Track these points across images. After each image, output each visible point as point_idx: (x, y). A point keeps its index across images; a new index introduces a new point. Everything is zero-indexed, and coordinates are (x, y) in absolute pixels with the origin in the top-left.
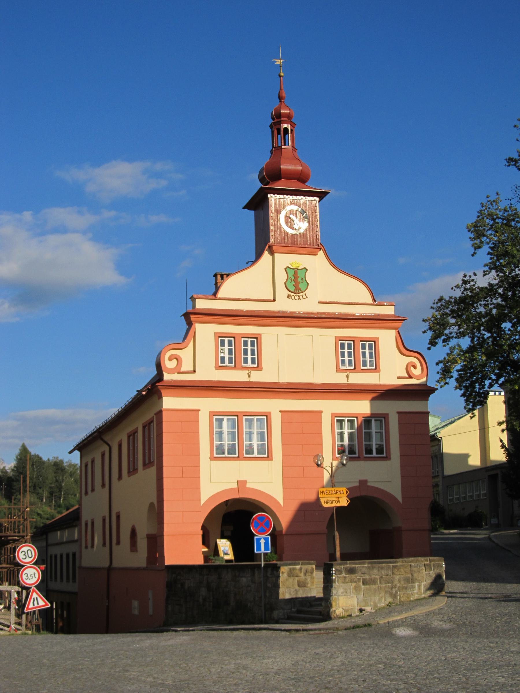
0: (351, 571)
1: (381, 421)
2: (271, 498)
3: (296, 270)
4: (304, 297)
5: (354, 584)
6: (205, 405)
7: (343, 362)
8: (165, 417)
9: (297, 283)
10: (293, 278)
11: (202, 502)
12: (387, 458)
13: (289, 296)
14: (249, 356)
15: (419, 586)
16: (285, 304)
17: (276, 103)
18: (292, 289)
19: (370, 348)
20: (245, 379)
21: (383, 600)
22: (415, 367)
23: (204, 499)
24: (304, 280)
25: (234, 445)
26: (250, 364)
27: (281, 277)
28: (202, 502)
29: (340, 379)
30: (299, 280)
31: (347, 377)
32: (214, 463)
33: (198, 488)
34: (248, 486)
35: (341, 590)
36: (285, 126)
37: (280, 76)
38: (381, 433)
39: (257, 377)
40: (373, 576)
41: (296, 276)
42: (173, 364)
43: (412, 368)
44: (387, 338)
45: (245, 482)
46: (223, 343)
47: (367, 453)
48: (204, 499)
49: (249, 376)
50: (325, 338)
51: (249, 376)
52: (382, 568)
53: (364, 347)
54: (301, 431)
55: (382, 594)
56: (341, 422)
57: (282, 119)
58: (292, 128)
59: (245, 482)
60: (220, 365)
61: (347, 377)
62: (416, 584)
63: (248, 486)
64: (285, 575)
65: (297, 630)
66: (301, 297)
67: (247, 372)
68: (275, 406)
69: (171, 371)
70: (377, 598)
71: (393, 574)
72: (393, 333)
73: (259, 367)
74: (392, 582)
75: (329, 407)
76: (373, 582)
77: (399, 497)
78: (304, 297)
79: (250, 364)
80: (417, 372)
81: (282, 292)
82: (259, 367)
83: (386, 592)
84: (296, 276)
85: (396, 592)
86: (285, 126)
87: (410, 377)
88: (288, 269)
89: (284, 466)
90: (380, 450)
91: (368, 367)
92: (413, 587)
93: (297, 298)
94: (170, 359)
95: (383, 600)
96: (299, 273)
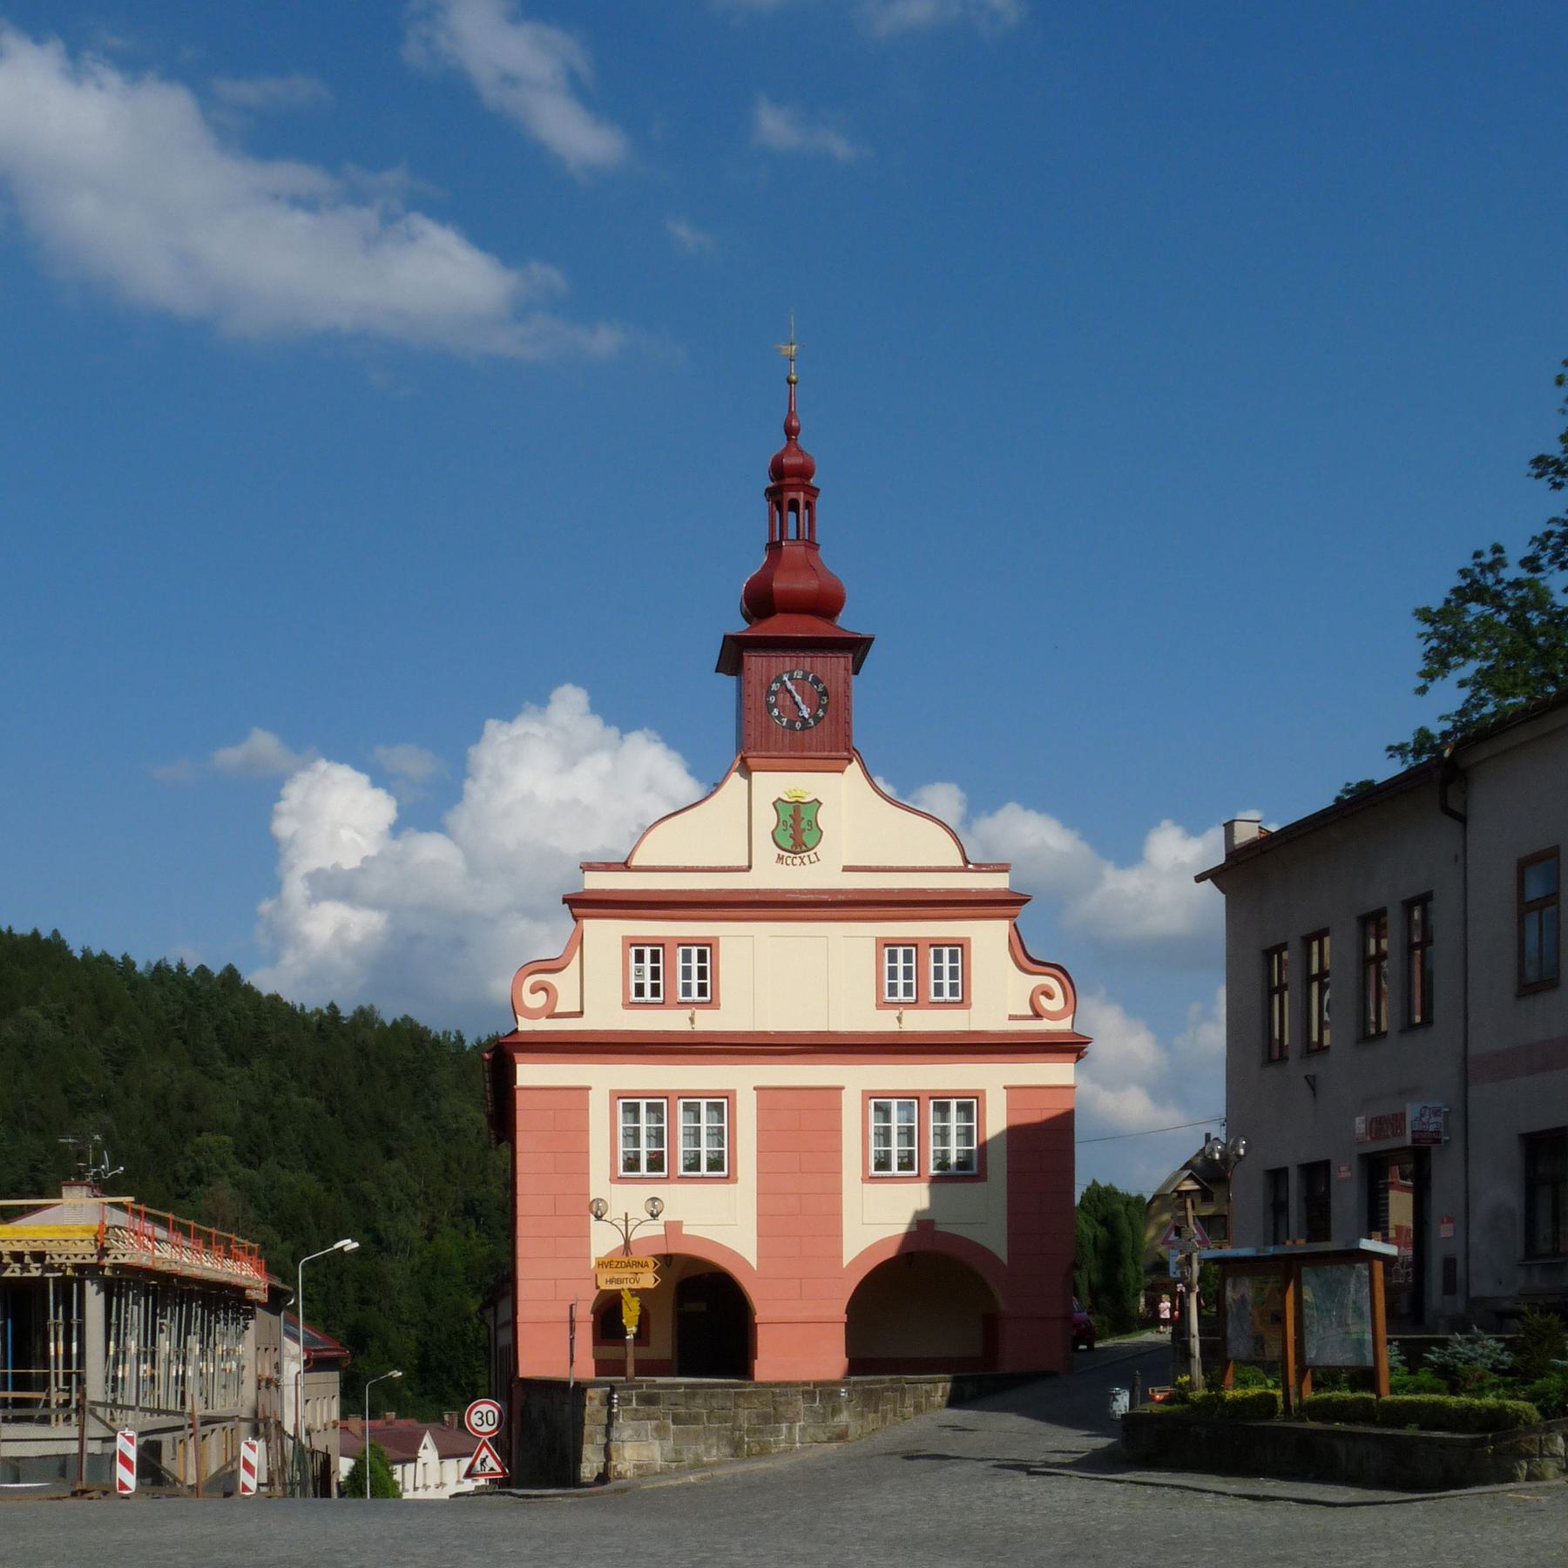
0: (649, 1400)
1: (911, 1104)
2: (733, 1254)
3: (797, 806)
4: (813, 858)
5: (654, 1423)
6: (602, 1080)
7: (893, 990)
8: (521, 1101)
9: (798, 829)
10: (790, 822)
11: (846, 1260)
12: (730, 1179)
13: (780, 858)
14: (901, 981)
15: (790, 1429)
16: (773, 874)
17: (782, 441)
18: (788, 843)
19: (953, 958)
20: (685, 1026)
21: (714, 1452)
22: (1049, 995)
23: (847, 1258)
24: (813, 824)
25: (911, 1153)
26: (901, 996)
27: (766, 820)
28: (846, 1260)
29: (885, 1023)
30: (804, 825)
31: (899, 1019)
32: (869, 1187)
33: (838, 1235)
34: (685, 1231)
35: (627, 1433)
36: (792, 495)
37: (790, 382)
38: (911, 1129)
39: (707, 1022)
40: (695, 1410)
41: (796, 817)
42: (539, 1000)
43: (1043, 999)
44: (988, 938)
45: (679, 1224)
46: (640, 957)
47: (687, 1168)
48: (847, 1258)
49: (692, 1020)
50: (856, 942)
51: (692, 1020)
52: (713, 1396)
53: (687, 957)
54: (800, 1131)
55: (713, 1440)
56: (632, 1110)
57: (788, 481)
58: (810, 499)
59: (679, 1224)
60: (887, 998)
61: (899, 1019)
62: (784, 1426)
63: (685, 1231)
64: (596, 1402)
65: (528, 1496)
66: (806, 860)
67: (896, 1013)
68: (743, 1080)
69: (533, 1014)
70: (701, 1448)
71: (737, 1406)
72: (1001, 928)
73: (713, 1004)
74: (734, 1419)
75: (856, 1080)
76: (695, 1419)
77: (1002, 1253)
78: (813, 858)
79: (901, 996)
80: (1056, 1004)
81: (766, 850)
82: (713, 1004)
83: (720, 1438)
84: (796, 817)
85: (742, 1438)
86: (792, 495)
87: (1037, 1015)
88: (779, 805)
89: (762, 1193)
90: (716, 1164)
91: (947, 996)
92: (777, 1432)
93: (797, 861)
94: (533, 991)
95: (714, 1452)
96: (806, 813)
